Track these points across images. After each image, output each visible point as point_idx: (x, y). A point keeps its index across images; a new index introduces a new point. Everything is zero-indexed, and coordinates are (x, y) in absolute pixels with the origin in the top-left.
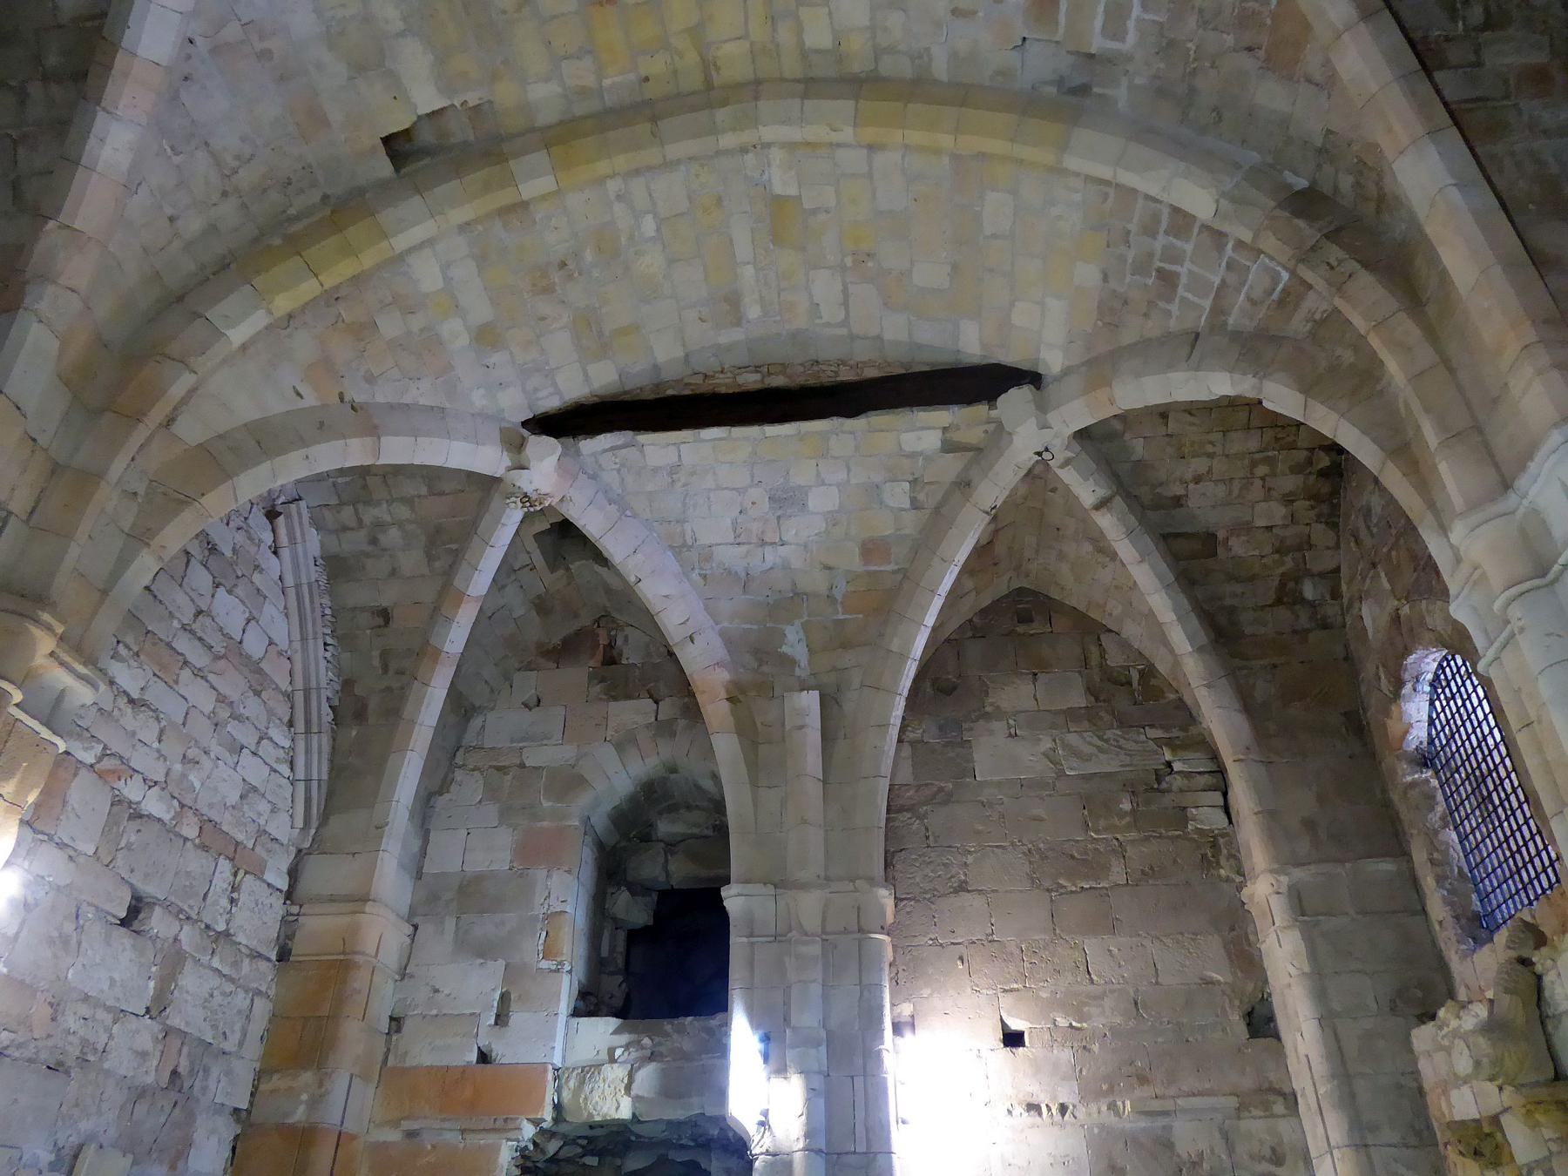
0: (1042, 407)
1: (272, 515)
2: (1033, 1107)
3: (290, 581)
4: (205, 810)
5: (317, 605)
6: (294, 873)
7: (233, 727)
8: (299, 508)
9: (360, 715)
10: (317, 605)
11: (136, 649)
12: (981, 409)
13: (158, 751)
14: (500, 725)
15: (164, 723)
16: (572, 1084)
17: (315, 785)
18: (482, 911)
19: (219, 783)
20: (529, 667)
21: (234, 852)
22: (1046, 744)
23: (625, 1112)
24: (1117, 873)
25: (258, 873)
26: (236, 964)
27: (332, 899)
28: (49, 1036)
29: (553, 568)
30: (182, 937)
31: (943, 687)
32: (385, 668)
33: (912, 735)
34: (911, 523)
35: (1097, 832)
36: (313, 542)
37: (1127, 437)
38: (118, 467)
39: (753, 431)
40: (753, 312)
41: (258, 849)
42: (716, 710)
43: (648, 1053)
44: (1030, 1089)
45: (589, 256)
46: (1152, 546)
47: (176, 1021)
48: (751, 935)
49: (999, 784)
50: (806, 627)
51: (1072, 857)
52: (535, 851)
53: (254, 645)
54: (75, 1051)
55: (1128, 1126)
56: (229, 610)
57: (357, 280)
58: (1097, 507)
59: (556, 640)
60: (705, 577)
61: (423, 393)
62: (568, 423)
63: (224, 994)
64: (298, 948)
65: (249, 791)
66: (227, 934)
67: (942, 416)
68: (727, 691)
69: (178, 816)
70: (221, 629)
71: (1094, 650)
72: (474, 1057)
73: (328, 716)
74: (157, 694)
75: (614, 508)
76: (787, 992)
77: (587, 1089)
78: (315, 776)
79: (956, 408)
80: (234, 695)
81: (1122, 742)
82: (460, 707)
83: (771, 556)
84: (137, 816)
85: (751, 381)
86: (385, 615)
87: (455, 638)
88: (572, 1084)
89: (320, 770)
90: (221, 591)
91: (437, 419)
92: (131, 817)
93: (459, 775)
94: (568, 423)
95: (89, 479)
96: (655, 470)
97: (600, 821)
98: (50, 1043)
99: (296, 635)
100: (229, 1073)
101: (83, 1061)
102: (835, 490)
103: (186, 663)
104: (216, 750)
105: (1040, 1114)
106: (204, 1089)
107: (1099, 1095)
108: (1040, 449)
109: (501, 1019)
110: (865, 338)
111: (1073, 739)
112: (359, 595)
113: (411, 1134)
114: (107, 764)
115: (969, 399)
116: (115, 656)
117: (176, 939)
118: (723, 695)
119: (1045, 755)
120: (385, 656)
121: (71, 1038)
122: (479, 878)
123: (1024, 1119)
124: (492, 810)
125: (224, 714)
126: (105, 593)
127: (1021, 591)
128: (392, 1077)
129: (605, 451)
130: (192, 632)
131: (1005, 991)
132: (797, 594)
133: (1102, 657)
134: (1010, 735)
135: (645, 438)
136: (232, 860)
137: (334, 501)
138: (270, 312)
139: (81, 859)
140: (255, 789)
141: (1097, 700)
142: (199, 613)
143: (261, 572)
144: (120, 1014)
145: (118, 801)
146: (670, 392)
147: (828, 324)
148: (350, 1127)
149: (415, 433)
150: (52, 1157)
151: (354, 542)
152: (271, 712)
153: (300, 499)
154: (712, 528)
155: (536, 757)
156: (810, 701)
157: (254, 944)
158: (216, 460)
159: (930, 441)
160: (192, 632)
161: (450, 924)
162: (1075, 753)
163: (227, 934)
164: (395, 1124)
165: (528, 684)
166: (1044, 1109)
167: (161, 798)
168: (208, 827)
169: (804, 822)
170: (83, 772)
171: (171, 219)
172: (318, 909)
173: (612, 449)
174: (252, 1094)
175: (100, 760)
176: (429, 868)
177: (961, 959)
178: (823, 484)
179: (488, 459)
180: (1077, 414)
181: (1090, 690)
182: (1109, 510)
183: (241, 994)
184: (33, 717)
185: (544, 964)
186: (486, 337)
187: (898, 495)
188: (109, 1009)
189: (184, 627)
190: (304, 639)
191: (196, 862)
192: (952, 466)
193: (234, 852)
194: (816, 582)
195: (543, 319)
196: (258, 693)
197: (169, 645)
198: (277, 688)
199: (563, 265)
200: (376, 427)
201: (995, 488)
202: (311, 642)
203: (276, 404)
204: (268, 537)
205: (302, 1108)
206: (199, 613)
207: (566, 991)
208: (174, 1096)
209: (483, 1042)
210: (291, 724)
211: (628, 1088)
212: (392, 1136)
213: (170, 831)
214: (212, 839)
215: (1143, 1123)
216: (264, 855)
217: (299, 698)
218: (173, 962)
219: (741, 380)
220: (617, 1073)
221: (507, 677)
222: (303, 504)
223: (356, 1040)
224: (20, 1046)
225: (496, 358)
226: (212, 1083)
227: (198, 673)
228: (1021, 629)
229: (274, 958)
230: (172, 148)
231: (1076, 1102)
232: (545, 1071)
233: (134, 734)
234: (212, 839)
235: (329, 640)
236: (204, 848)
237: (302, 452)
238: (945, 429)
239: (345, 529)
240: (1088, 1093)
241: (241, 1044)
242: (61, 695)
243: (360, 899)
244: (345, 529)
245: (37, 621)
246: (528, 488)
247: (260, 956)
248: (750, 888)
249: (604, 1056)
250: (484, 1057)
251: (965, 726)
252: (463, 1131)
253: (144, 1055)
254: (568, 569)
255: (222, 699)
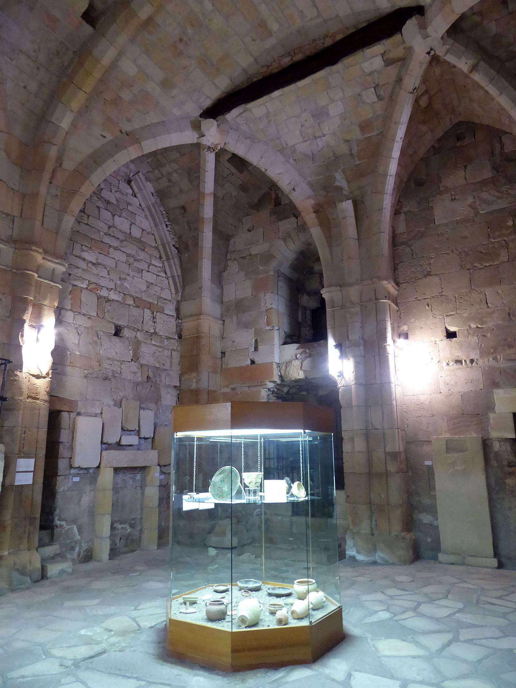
0: (423, 27)
1: (129, 182)
2: (458, 362)
3: (144, 205)
4: (134, 294)
5: (158, 211)
6: (178, 310)
7: (136, 264)
8: (139, 176)
9: (187, 248)
10: (158, 211)
11: (89, 246)
12: (397, 37)
13: (109, 278)
14: (240, 241)
15: (108, 269)
16: (283, 368)
17: (176, 277)
18: (244, 312)
19: (137, 285)
20: (248, 215)
21: (150, 306)
22: (470, 200)
23: (301, 375)
24: (504, 256)
25: (162, 311)
26: (162, 342)
27: (191, 316)
28: (100, 370)
29: (241, 172)
30: (138, 336)
31: (416, 183)
32: (190, 229)
33: (405, 209)
34: (379, 108)
35: (494, 239)
36: (150, 187)
37: (485, 23)
38: (43, 189)
39: (292, 87)
40: (275, 27)
41: (159, 303)
42: (310, 218)
43: (308, 355)
44: (458, 354)
45: (190, 31)
46: (507, 84)
47: (143, 362)
48: (334, 307)
49: (446, 225)
50: (344, 171)
51: (481, 252)
52: (259, 287)
53: (136, 233)
54: (110, 374)
55: (502, 366)
56: (122, 223)
57: (102, 81)
58: (471, 72)
59: (256, 201)
60: (295, 160)
61: (152, 118)
62: (216, 110)
63: (159, 352)
64: (184, 334)
65: (149, 285)
66: (155, 333)
67: (378, 48)
68: (314, 208)
69: (124, 299)
70: (121, 231)
71: (498, 146)
72: (249, 362)
73: (174, 251)
74: (102, 259)
75: (248, 141)
76: (347, 326)
77: (288, 369)
78: (176, 274)
79: (384, 42)
80: (134, 253)
81: (510, 191)
82: (222, 237)
83: (320, 143)
84: (108, 300)
85: (286, 61)
86: (183, 208)
87: (208, 211)
88: (283, 368)
89: (177, 271)
90: (116, 217)
91: (163, 126)
92: (106, 302)
93: (230, 263)
94: (216, 110)
95: (35, 195)
96: (260, 118)
97: (286, 269)
98: (101, 372)
99: (153, 225)
100: (169, 375)
101: (114, 377)
102: (339, 102)
103: (110, 246)
104: (132, 274)
105: (462, 364)
106: (161, 381)
107: (489, 354)
108: (428, 50)
109: (256, 349)
110: (332, 19)
111: (485, 195)
112: (173, 203)
113: (233, 389)
114: (91, 286)
115: (389, 34)
116: (82, 250)
117: (136, 337)
118: (311, 210)
119: (470, 206)
120: (188, 224)
121: (108, 370)
122: (242, 300)
123: (453, 366)
124: (242, 274)
125: (131, 260)
126: (57, 233)
127: (459, 124)
128: (226, 372)
129: (237, 116)
130: (109, 235)
131: (447, 316)
132: (336, 157)
133: (502, 148)
134: (452, 200)
135: (250, 105)
136: (150, 309)
137: (150, 169)
138: (72, 111)
139: (92, 318)
140: (152, 284)
141: (498, 172)
142: (110, 227)
143: (131, 205)
144: (122, 362)
145: (99, 298)
146: (255, 80)
147: (311, 19)
148: (211, 388)
149: (154, 136)
150: (114, 403)
151: (164, 183)
152: (151, 255)
153: (139, 172)
154: (292, 137)
155: (255, 250)
156: (347, 206)
157: (167, 335)
158: (81, 173)
159: (378, 63)
160: (109, 235)
161: (235, 317)
162: (484, 201)
163: (155, 333)
164: (227, 386)
165: (248, 221)
166: (464, 362)
167: (115, 294)
168: (136, 300)
169: (349, 258)
170: (83, 291)
171: (25, 87)
172: (186, 320)
173: (241, 114)
174: (180, 381)
175: (88, 285)
176: (225, 300)
177: (428, 305)
178: (334, 101)
179: (189, 137)
180: (439, 24)
181: (495, 168)
182: (477, 71)
183: (166, 351)
184: (46, 280)
185: (268, 328)
186: (166, 85)
187: (370, 96)
188: (118, 361)
189: (105, 234)
190: (156, 225)
191: (136, 312)
192: (392, 71)
193: (150, 306)
194: (344, 149)
195: (185, 68)
196: (143, 250)
197: (102, 242)
198: (151, 246)
199: (181, 40)
200: (137, 139)
201: (413, 79)
202: (160, 226)
203: (97, 144)
204: (130, 191)
205: (194, 384)
206: (110, 227)
207: (277, 337)
208: (150, 384)
209: (251, 357)
210: (161, 257)
211: (301, 368)
212: (228, 390)
213: (122, 304)
214: (139, 303)
215: (509, 364)
216: (162, 305)
217: (161, 248)
218: (137, 345)
219: (282, 63)
220: (297, 363)
221: (240, 221)
222: (140, 174)
223: (206, 362)
224: (91, 374)
225: (175, 92)
226: (163, 379)
227: (116, 249)
228: (458, 144)
229: (177, 338)
230: (10, 59)
231: (478, 358)
232: (272, 364)
233: (98, 275)
234: (139, 303)
235: (168, 223)
236: (138, 307)
237: (112, 159)
238: (383, 55)
239: (159, 179)
240: (483, 354)
241: (171, 366)
242: (54, 270)
243: (199, 314)
244: (159, 179)
245: (32, 250)
246: (209, 144)
247: (171, 338)
248: (330, 289)
249: (294, 357)
250: (253, 362)
251: (430, 199)
252: (249, 387)
253: (135, 373)
254: (248, 170)
255: (128, 255)
